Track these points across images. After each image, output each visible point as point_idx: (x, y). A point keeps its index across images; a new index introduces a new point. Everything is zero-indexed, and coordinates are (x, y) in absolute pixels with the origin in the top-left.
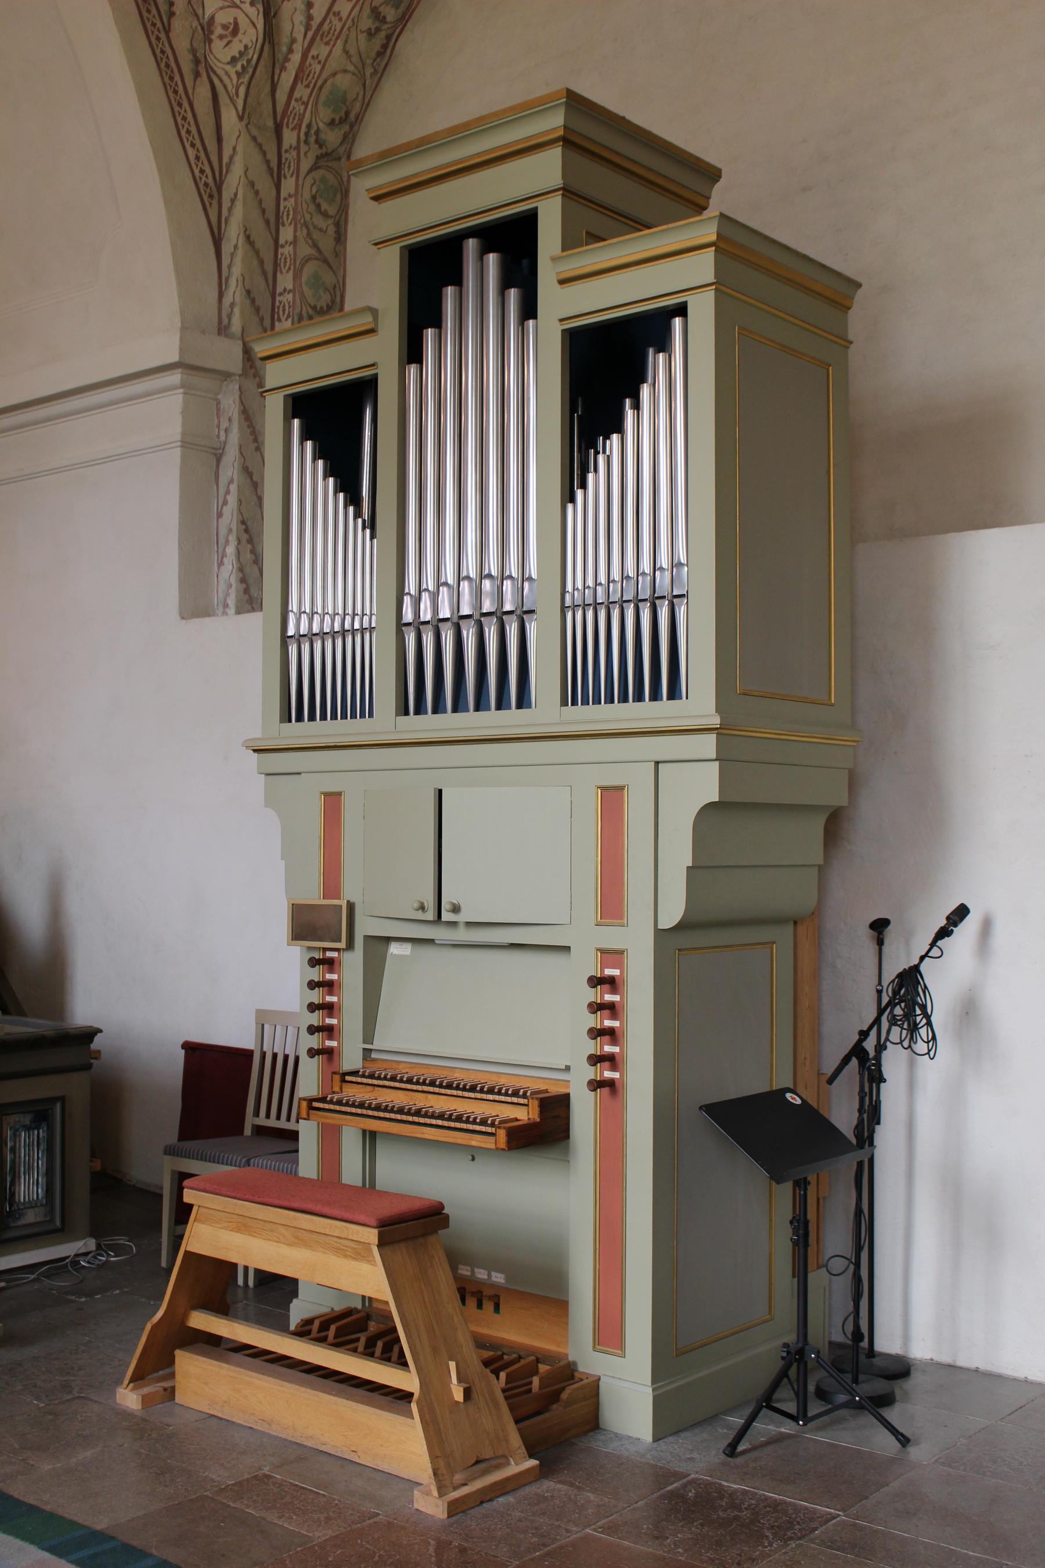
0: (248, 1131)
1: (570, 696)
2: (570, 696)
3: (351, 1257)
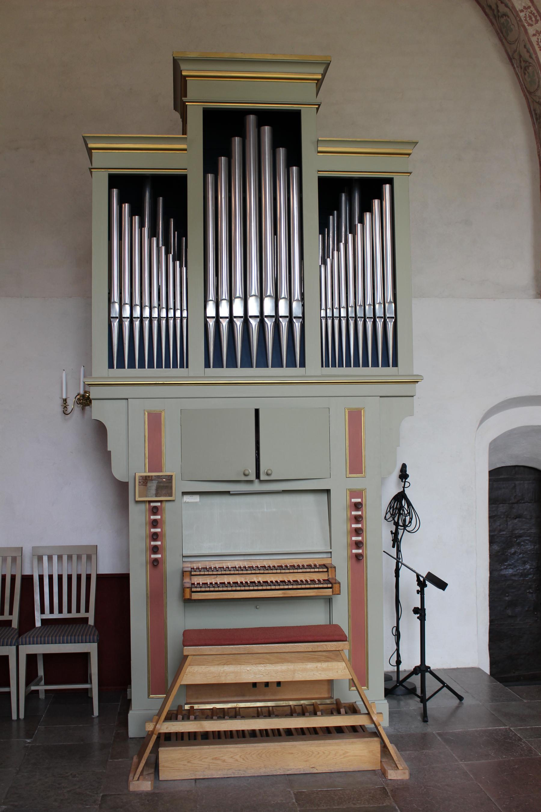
0: (38, 624)
1: (325, 363)
2: (325, 363)
3: (323, 661)
